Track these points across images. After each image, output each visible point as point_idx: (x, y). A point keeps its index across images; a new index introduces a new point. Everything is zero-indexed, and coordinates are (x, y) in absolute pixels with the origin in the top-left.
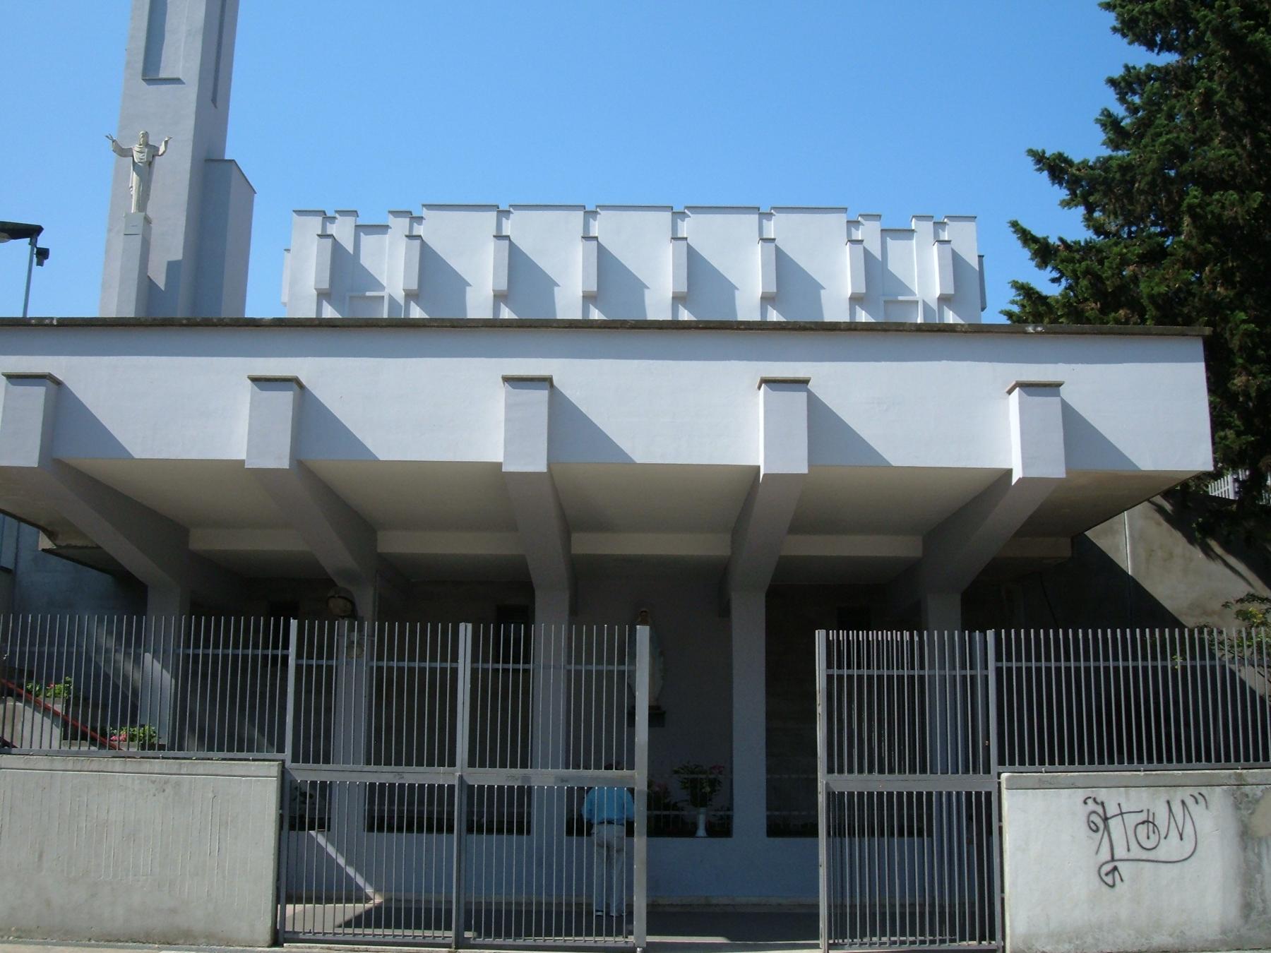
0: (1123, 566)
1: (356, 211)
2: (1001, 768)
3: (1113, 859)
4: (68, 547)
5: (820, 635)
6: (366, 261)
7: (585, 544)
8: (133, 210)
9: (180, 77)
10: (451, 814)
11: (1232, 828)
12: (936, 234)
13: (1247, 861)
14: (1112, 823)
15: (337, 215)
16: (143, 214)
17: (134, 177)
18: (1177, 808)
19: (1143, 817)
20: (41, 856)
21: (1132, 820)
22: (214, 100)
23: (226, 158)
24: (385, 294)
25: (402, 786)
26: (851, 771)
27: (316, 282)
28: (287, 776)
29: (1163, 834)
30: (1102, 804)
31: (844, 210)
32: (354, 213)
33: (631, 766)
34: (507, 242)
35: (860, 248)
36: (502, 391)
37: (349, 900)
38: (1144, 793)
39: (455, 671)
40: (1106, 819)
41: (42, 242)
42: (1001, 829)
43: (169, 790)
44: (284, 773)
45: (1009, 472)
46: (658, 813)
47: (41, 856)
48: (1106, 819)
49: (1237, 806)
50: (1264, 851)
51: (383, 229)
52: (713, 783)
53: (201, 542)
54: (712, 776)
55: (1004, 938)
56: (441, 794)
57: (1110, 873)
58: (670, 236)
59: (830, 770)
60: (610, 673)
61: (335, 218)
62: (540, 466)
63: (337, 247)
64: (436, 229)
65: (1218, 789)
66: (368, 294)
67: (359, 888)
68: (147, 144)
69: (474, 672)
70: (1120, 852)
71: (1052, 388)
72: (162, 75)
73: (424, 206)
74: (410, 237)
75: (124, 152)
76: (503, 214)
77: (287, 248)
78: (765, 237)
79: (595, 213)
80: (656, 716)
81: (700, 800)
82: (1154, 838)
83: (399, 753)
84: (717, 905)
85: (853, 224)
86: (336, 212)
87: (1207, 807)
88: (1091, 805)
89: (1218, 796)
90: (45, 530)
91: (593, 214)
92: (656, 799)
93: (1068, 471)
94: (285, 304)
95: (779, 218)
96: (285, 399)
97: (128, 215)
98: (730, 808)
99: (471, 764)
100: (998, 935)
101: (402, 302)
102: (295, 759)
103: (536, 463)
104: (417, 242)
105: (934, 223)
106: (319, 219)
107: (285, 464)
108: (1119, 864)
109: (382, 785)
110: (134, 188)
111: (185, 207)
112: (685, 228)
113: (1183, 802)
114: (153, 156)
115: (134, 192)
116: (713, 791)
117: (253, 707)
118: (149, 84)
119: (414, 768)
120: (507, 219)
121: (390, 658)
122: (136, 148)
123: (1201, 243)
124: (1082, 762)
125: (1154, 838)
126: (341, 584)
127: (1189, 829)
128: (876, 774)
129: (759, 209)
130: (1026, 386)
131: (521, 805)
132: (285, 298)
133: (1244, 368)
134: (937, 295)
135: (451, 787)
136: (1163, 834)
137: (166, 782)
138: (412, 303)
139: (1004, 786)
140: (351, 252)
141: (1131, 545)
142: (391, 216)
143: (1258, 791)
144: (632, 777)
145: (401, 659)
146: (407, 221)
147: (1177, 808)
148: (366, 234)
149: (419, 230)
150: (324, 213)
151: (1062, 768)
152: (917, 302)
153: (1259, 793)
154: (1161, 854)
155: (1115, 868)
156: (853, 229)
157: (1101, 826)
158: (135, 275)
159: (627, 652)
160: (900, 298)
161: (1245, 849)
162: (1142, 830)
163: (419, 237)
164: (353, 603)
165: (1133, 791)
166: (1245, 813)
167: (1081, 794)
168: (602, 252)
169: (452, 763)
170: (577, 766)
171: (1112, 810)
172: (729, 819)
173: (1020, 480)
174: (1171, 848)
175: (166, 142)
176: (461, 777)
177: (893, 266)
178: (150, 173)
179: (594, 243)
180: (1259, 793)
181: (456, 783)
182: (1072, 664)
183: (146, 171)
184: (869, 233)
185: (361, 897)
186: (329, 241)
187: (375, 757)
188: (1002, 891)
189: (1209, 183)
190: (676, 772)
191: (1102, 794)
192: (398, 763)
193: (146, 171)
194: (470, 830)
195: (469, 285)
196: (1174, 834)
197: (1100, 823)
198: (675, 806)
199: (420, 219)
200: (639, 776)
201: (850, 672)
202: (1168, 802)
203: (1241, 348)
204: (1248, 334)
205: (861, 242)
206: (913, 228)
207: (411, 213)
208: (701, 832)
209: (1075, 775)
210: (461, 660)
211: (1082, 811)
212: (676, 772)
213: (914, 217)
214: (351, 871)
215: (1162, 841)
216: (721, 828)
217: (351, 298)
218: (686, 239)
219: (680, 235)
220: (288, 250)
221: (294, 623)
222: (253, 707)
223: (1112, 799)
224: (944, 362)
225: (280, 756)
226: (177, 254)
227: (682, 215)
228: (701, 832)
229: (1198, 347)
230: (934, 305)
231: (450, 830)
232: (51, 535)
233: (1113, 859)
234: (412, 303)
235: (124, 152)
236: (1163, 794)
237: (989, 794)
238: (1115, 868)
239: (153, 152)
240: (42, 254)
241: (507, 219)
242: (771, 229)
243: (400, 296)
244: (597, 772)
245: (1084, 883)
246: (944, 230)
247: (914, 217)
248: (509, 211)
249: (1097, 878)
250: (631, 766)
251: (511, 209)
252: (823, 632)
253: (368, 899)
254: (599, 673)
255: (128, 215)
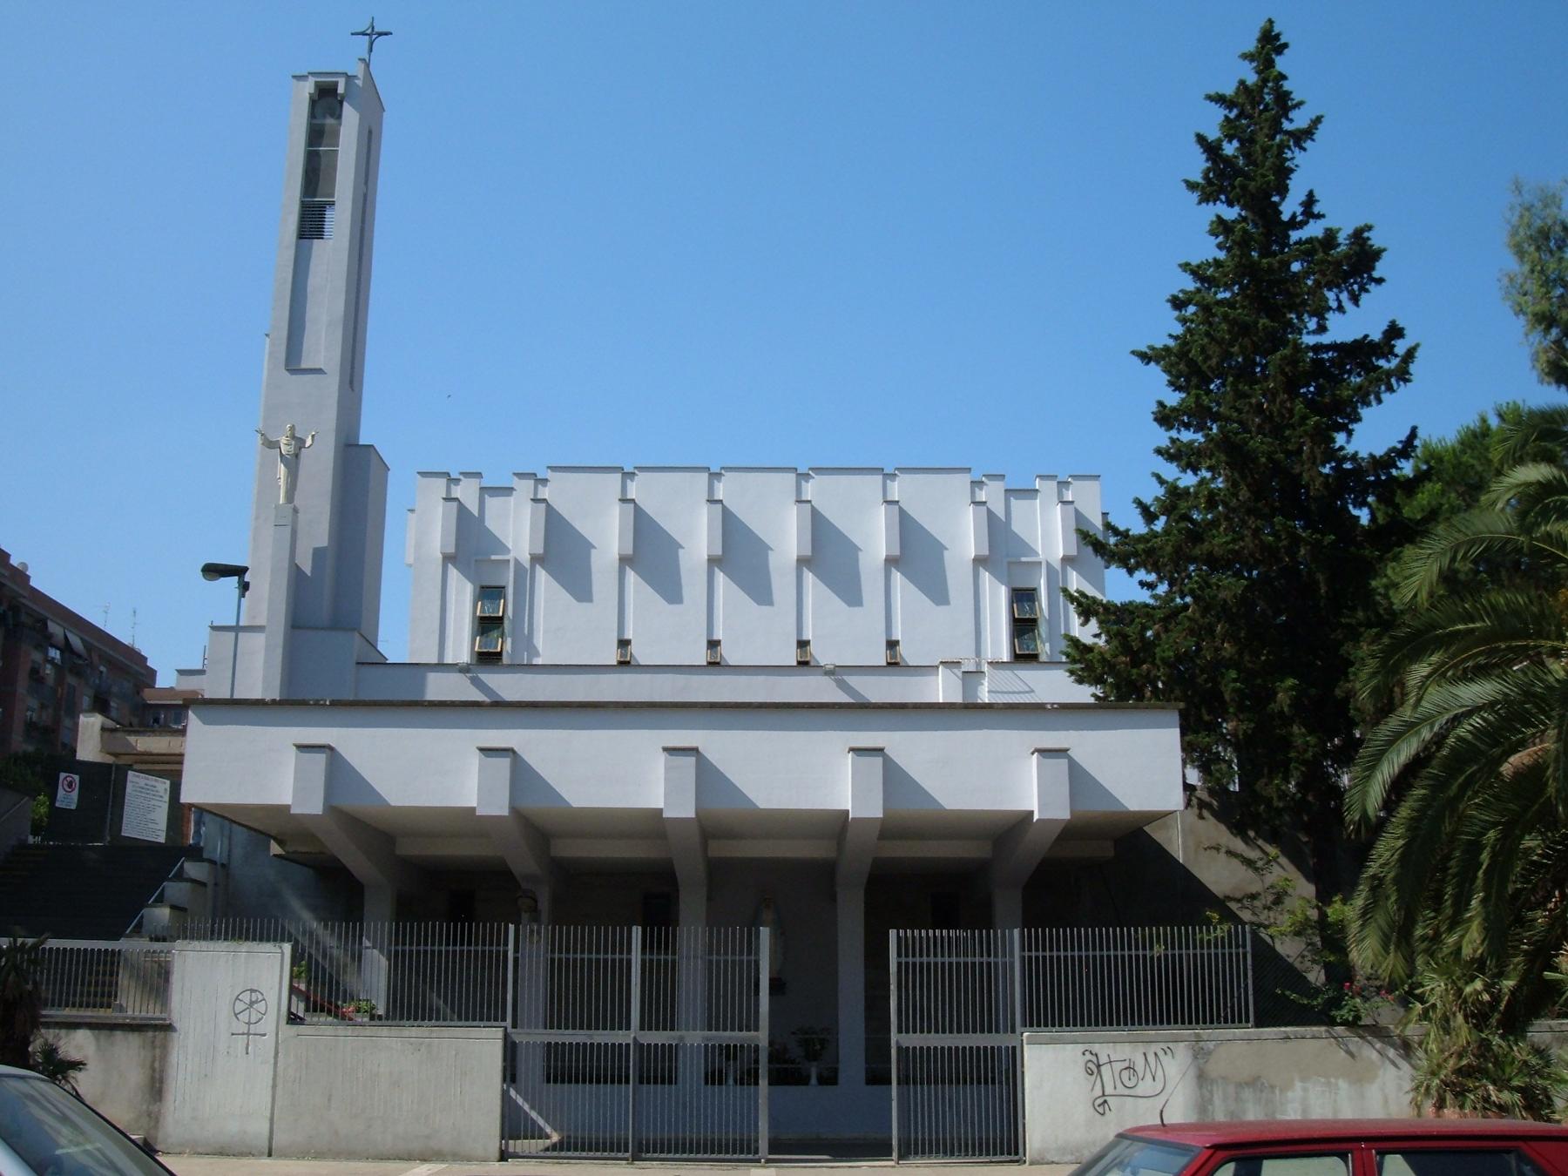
0: (1175, 856)
1: (480, 473)
2: (1023, 1029)
3: (1104, 1095)
4: (295, 852)
5: (893, 933)
6: (491, 523)
7: (719, 850)
8: (282, 501)
9: (322, 367)
10: (628, 1068)
11: (1192, 1072)
12: (1060, 494)
13: (1202, 1096)
14: (1103, 1068)
15: (461, 477)
16: (292, 505)
17: (282, 469)
18: (1151, 1058)
19: (1126, 1064)
20: (329, 1100)
21: (1118, 1066)
22: (351, 382)
23: (361, 443)
24: (510, 557)
25: (592, 1044)
26: (915, 1032)
27: (442, 547)
28: (508, 1039)
29: (1141, 1076)
30: (1096, 1055)
31: (968, 470)
32: (478, 475)
33: (757, 1029)
34: (632, 505)
35: (1070, 508)
36: (662, 756)
37: (540, 1138)
38: (1127, 1048)
39: (629, 962)
40: (1099, 1066)
41: (247, 578)
42: (1023, 1073)
43: (423, 1049)
44: (506, 1036)
45: (1032, 813)
46: (778, 1066)
47: (329, 1100)
48: (1099, 1066)
49: (1195, 1057)
50: (1215, 1088)
51: (508, 491)
52: (823, 1042)
53: (407, 849)
54: (822, 1036)
55: (1025, 1155)
56: (622, 1050)
57: (1101, 1105)
58: (794, 499)
59: (900, 1031)
60: (741, 962)
61: (459, 480)
62: (691, 814)
63: (462, 510)
64: (560, 492)
65: (1182, 1044)
66: (493, 557)
67: (541, 1129)
68: (293, 437)
69: (643, 962)
70: (1109, 1090)
71: (1061, 752)
72: (304, 366)
73: (548, 467)
74: (535, 500)
75: (272, 445)
76: (628, 476)
77: (410, 508)
78: (889, 499)
79: (720, 474)
80: (777, 986)
81: (813, 1056)
82: (1134, 1080)
83: (567, 1019)
84: (826, 1139)
85: (977, 484)
86: (461, 473)
87: (1173, 1057)
88: (1088, 1056)
89: (1182, 1050)
90: (276, 839)
91: (718, 476)
92: (777, 1055)
93: (1072, 812)
94: (410, 566)
95: (903, 478)
96: (504, 763)
97: (277, 507)
98: (837, 1062)
99: (642, 1028)
100: (1021, 1151)
101: (527, 565)
102: (514, 1026)
103: (688, 811)
104: (543, 506)
105: (1059, 483)
106: (443, 481)
107: (505, 812)
108: (1107, 1098)
109: (578, 1044)
110: (282, 480)
111: (330, 494)
112: (810, 490)
113: (1156, 1054)
114: (300, 448)
115: (282, 483)
116: (823, 1048)
117: (439, 982)
118: (292, 374)
119: (601, 1032)
120: (632, 481)
121: (582, 952)
122: (283, 440)
123: (1203, 617)
124: (1082, 1025)
125: (1134, 1080)
126: (524, 885)
127: (1159, 1073)
128: (904, 1034)
129: (883, 469)
130: (1043, 752)
131: (670, 1060)
132: (411, 560)
133: (1235, 715)
134: (1061, 555)
135: (628, 1045)
136: (1141, 1076)
137: (421, 1044)
138: (538, 566)
139: (1025, 1042)
140: (477, 515)
141: (1182, 837)
142: (516, 478)
143: (1211, 1045)
144: (758, 1037)
145: (590, 952)
146: (532, 482)
147: (1151, 1058)
148: (1016, 499)
149: (544, 493)
150: (448, 474)
151: (1068, 1029)
152: (1040, 563)
153: (1212, 1047)
154: (1139, 1091)
155: (1105, 1101)
156: (977, 489)
157: (1095, 1070)
158: (286, 564)
159: (752, 947)
160: (1023, 559)
161: (1200, 1087)
162: (1125, 1074)
163: (544, 500)
164: (536, 902)
165: (1118, 1046)
166: (1201, 1061)
167: (1081, 1047)
168: (727, 516)
169: (628, 1028)
170: (717, 1029)
171: (1103, 1059)
172: (836, 1071)
173: (1037, 820)
174: (1146, 1087)
175: (313, 436)
176: (635, 1038)
177: (1016, 527)
178: (297, 464)
179: (719, 506)
180: (1212, 1047)
181: (631, 1042)
182: (1076, 953)
183: (293, 462)
184: (992, 493)
185: (543, 1135)
186: (455, 504)
187: (551, 1023)
188: (1024, 1118)
189: (1214, 563)
190: (793, 1033)
191: (1096, 1048)
192: (589, 1028)
193: (293, 462)
194: (641, 1082)
195: (594, 547)
196: (1149, 1077)
197: (1094, 1068)
198: (793, 1062)
199: (545, 481)
200: (762, 1037)
201: (907, 960)
202: (1145, 1054)
203: (1232, 700)
204: (1234, 690)
205: (984, 503)
206: (1037, 487)
207: (535, 475)
208: (814, 1081)
209: (1077, 1034)
210: (633, 953)
211: (1082, 1060)
212: (793, 1033)
213: (1038, 476)
214: (534, 1114)
215: (1140, 1082)
216: (829, 1078)
217: (476, 561)
218: (810, 501)
219: (804, 498)
220: (412, 511)
221: (511, 927)
222: (439, 982)
223: (1104, 1051)
224: (985, 731)
225: (503, 1024)
226: (323, 540)
227: (806, 476)
228: (814, 1081)
229: (1175, 717)
230: (1057, 565)
231: (627, 1082)
232: (280, 843)
233: (1104, 1095)
234: (538, 566)
235: (272, 445)
236: (1141, 1048)
237: (1014, 1048)
238: (1105, 1101)
239: (300, 443)
240: (245, 587)
241: (632, 481)
242: (895, 490)
243: (525, 559)
244: (733, 1033)
245: (1082, 1110)
246: (1068, 490)
247: (1038, 476)
248: (634, 473)
249: (1092, 1108)
250: (757, 1029)
251: (636, 471)
252: (895, 931)
253: (548, 1137)
254: (733, 962)
255: (277, 507)
